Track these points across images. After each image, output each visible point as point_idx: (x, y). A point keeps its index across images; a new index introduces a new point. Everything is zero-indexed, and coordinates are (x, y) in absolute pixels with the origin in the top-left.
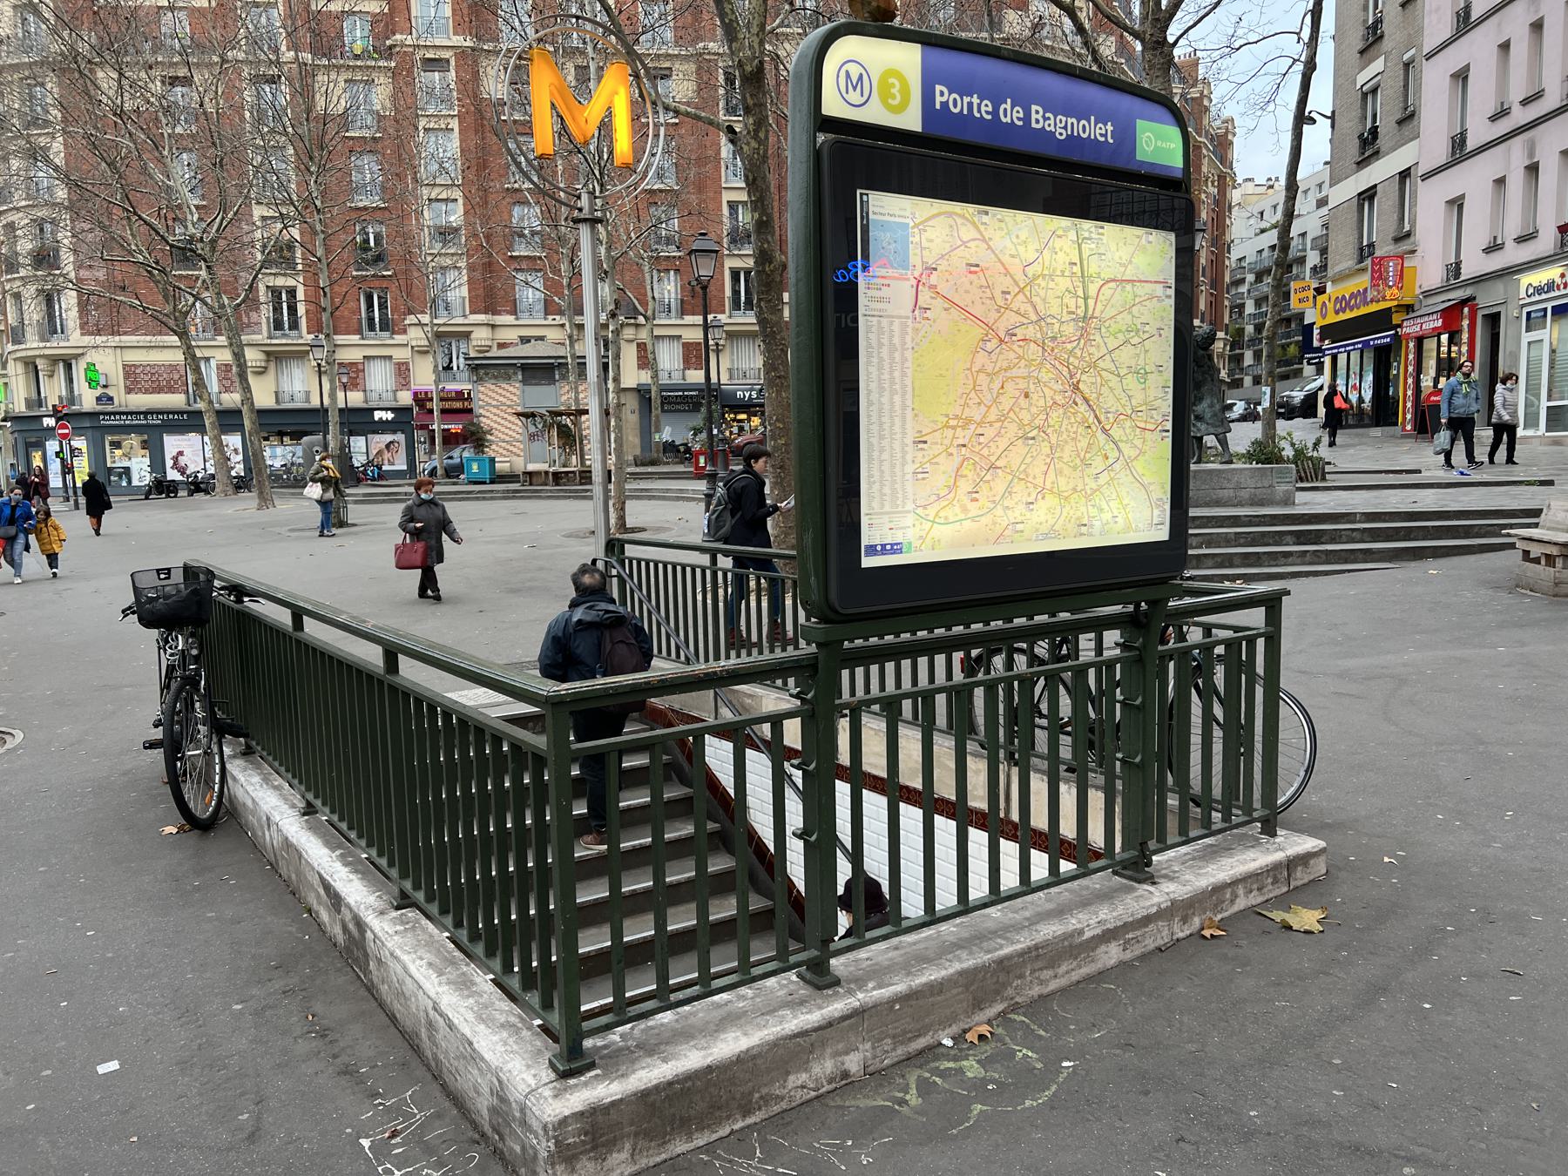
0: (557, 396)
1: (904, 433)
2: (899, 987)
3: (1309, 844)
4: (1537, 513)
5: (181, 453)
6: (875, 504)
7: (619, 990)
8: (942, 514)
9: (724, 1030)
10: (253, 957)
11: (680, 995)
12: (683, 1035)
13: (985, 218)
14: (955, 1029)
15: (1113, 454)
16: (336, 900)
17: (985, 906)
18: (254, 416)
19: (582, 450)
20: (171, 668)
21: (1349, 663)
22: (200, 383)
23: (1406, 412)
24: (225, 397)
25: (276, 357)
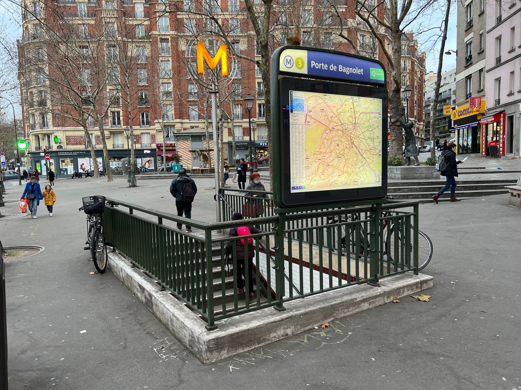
0: (203, 145)
1: (303, 156)
2: (302, 311)
3: (428, 277)
4: (516, 181)
5: (83, 164)
6: (295, 175)
7: (224, 308)
8: (314, 178)
9: (253, 320)
10: (120, 306)
11: (241, 310)
12: (242, 321)
13: (325, 97)
14: (319, 324)
15: (364, 162)
16: (143, 289)
17: (328, 290)
18: (107, 152)
19: (210, 162)
20: (91, 226)
21: (450, 227)
22: (90, 142)
23: (483, 149)
24: (97, 146)
25: (113, 133)
